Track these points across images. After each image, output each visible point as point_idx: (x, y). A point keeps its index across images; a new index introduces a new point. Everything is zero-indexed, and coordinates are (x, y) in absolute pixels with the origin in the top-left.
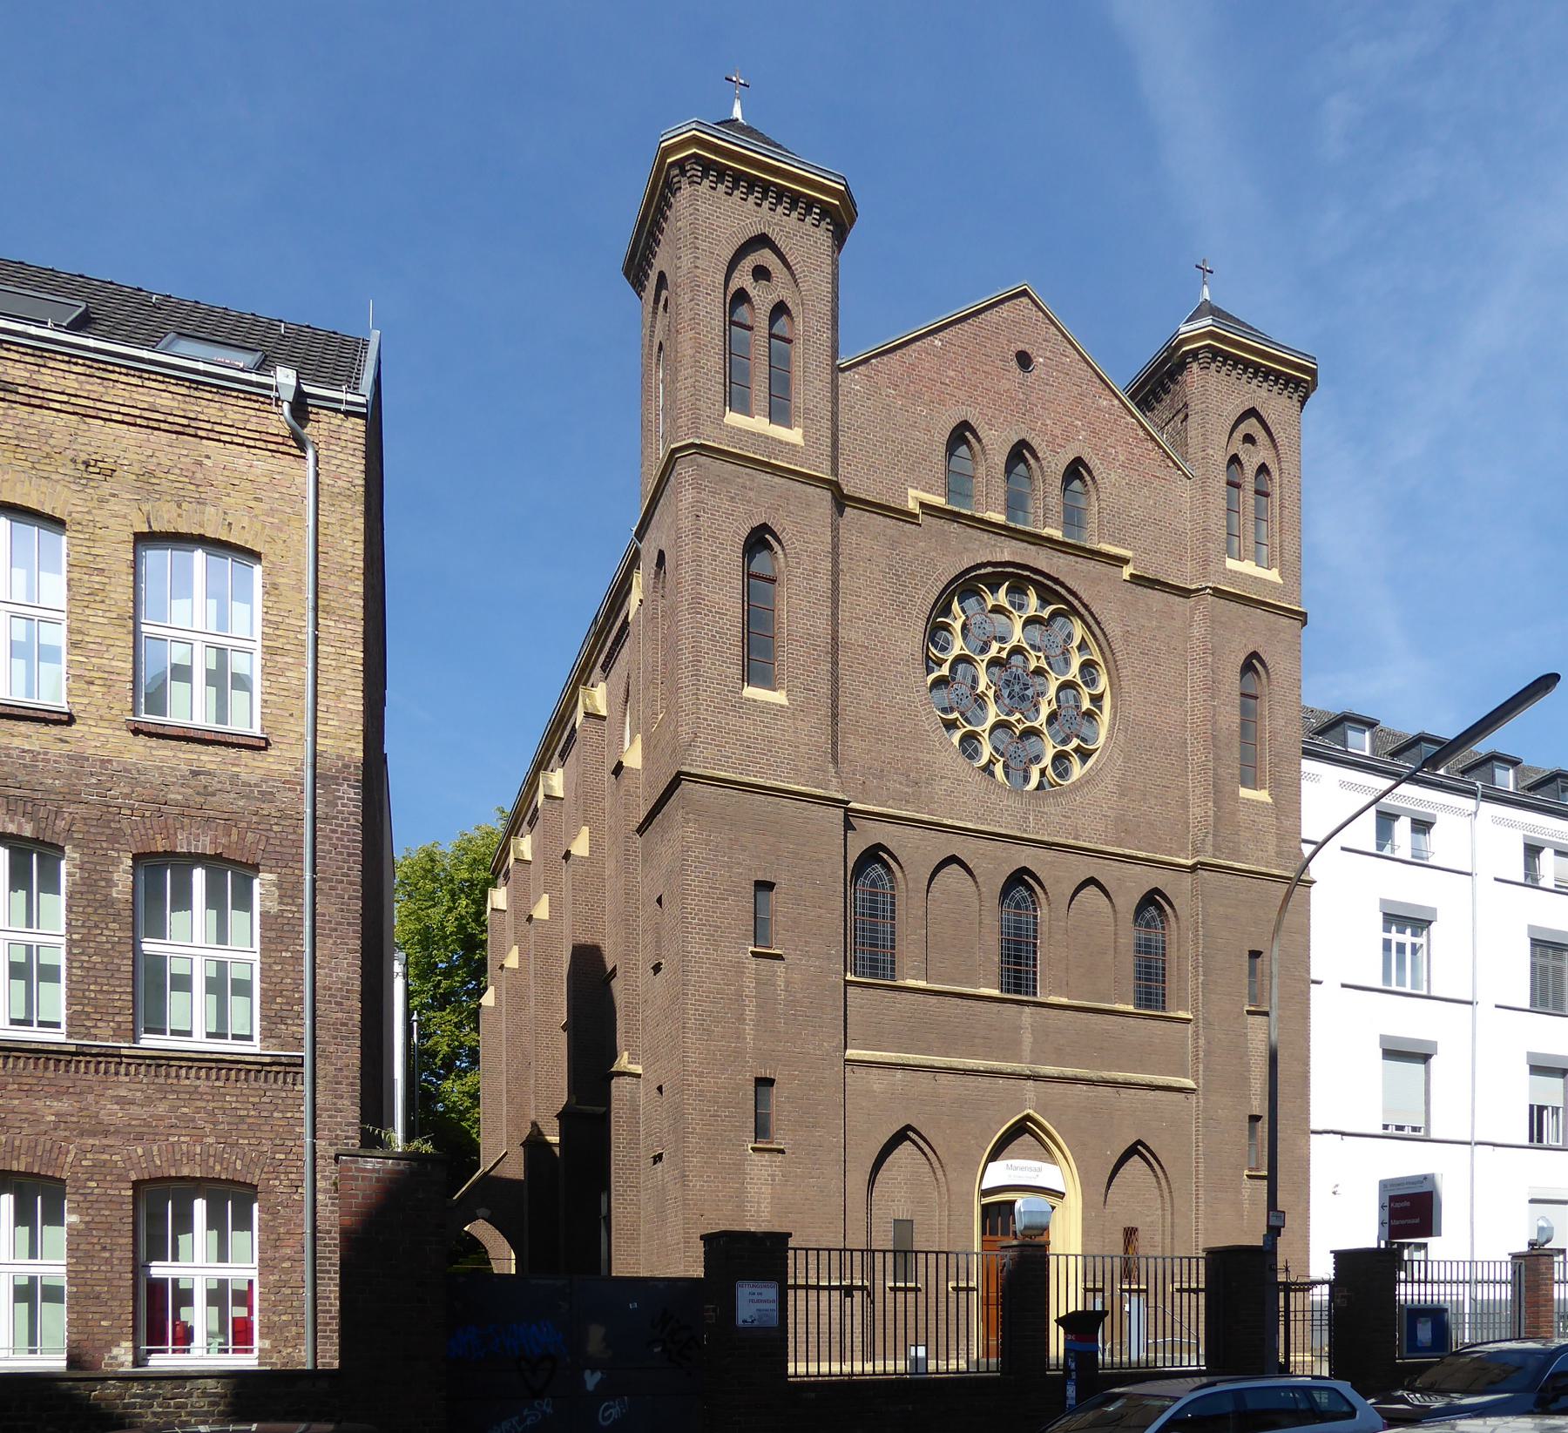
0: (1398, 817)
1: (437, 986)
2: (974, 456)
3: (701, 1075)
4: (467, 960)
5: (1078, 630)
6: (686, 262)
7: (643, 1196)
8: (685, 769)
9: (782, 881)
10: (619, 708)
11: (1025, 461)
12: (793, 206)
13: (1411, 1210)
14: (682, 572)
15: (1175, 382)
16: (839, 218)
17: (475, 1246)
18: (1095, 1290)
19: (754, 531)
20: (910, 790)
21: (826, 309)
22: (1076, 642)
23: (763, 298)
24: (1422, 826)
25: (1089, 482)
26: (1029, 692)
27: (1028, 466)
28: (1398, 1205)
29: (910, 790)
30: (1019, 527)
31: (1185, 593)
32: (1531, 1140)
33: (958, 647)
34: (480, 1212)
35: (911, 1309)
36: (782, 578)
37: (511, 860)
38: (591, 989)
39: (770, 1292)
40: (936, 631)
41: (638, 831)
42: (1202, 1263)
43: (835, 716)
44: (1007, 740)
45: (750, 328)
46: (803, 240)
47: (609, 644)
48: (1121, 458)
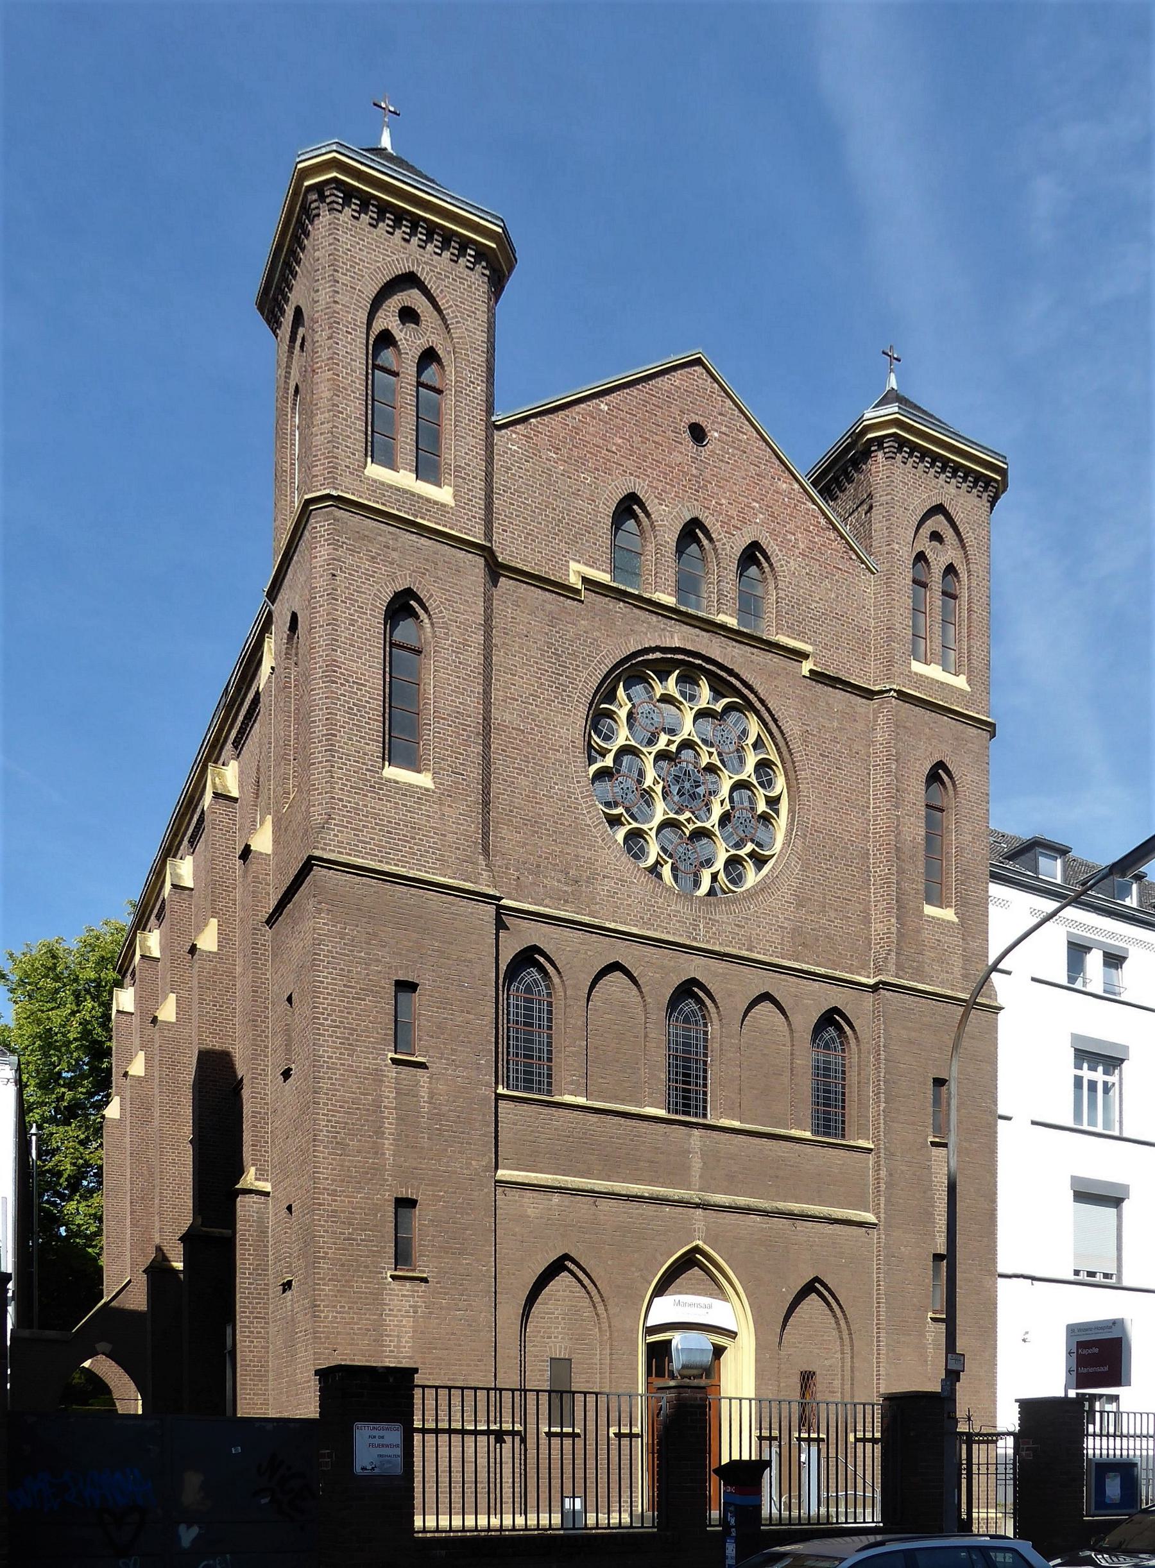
0: (1089, 949)
1: (61, 1098)
2: (642, 532)
3: (334, 1193)
4: (95, 1070)
5: (754, 728)
6: (324, 296)
7: (273, 1329)
8: (317, 853)
9: (426, 982)
10: (251, 789)
11: (698, 542)
12: (445, 244)
13: (1100, 1356)
14: (316, 636)
15: (858, 470)
16: (497, 264)
17: (99, 1387)
18: (771, 1439)
19: (397, 595)
20: (569, 889)
21: (481, 359)
22: (751, 739)
23: (410, 341)
24: (1114, 960)
25: (767, 570)
26: (701, 790)
27: (701, 546)
28: (1085, 1352)
29: (569, 889)
30: (690, 611)
31: (868, 694)
32: (1078, 1115)
33: (623, 736)
34: (100, 1346)
35: (568, 1456)
36: (429, 649)
37: (137, 957)
38: (217, 1094)
39: (393, 1435)
40: (599, 717)
41: (267, 922)
42: (878, 1411)
43: (486, 803)
44: (676, 840)
45: (395, 374)
46: (457, 284)
47: (240, 718)
48: (802, 546)
